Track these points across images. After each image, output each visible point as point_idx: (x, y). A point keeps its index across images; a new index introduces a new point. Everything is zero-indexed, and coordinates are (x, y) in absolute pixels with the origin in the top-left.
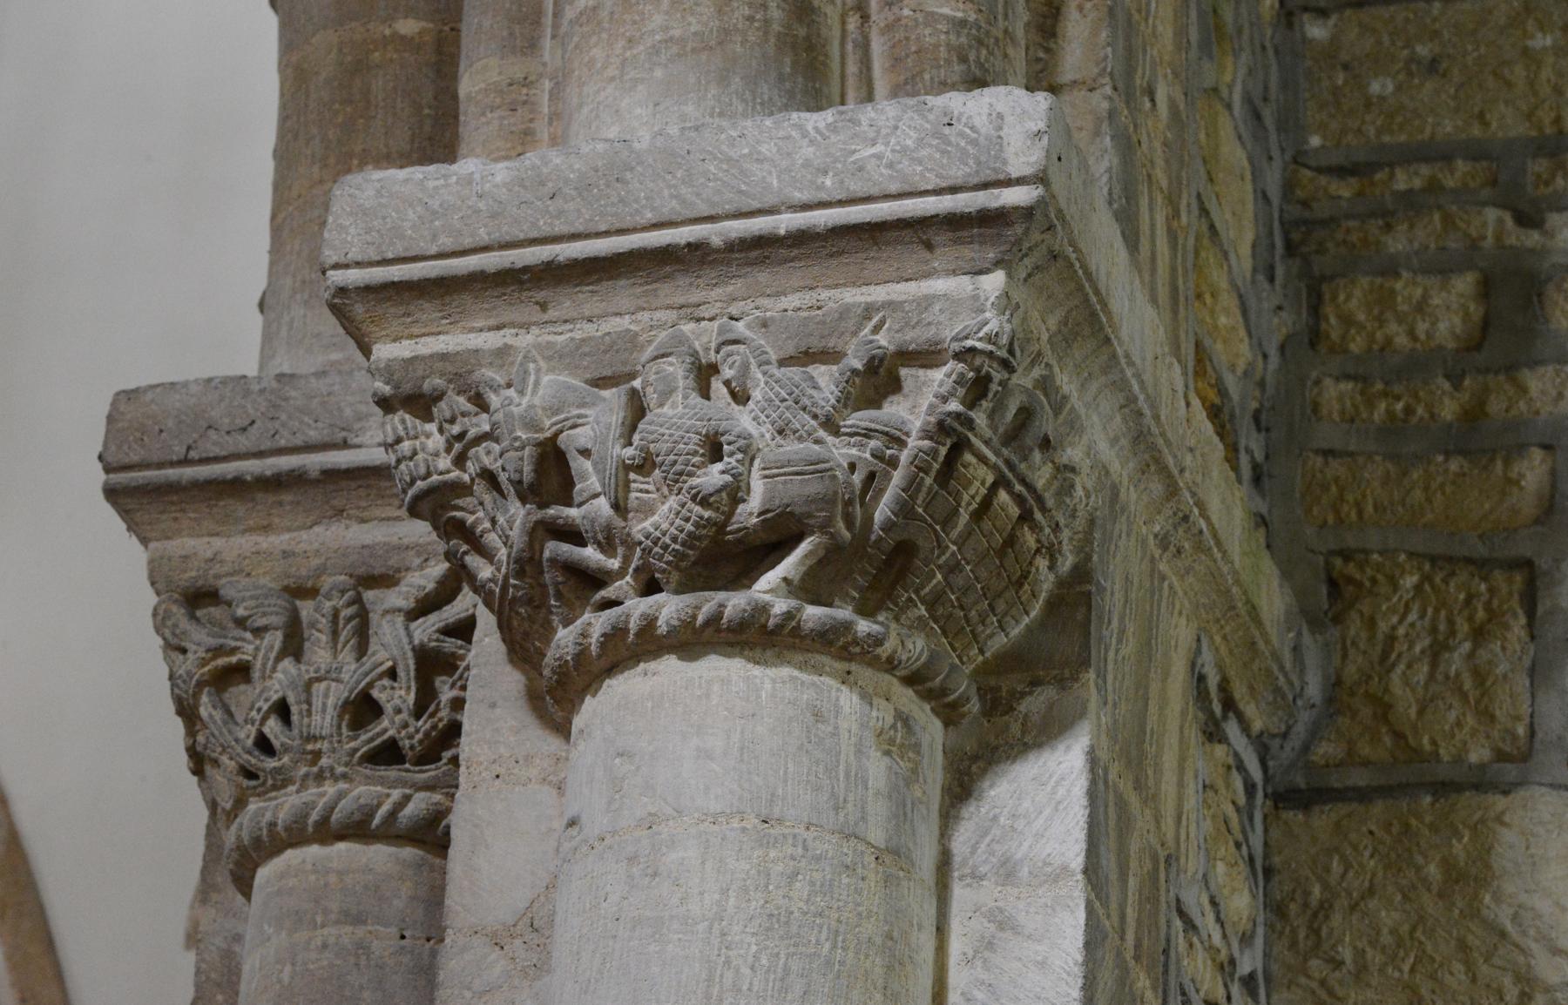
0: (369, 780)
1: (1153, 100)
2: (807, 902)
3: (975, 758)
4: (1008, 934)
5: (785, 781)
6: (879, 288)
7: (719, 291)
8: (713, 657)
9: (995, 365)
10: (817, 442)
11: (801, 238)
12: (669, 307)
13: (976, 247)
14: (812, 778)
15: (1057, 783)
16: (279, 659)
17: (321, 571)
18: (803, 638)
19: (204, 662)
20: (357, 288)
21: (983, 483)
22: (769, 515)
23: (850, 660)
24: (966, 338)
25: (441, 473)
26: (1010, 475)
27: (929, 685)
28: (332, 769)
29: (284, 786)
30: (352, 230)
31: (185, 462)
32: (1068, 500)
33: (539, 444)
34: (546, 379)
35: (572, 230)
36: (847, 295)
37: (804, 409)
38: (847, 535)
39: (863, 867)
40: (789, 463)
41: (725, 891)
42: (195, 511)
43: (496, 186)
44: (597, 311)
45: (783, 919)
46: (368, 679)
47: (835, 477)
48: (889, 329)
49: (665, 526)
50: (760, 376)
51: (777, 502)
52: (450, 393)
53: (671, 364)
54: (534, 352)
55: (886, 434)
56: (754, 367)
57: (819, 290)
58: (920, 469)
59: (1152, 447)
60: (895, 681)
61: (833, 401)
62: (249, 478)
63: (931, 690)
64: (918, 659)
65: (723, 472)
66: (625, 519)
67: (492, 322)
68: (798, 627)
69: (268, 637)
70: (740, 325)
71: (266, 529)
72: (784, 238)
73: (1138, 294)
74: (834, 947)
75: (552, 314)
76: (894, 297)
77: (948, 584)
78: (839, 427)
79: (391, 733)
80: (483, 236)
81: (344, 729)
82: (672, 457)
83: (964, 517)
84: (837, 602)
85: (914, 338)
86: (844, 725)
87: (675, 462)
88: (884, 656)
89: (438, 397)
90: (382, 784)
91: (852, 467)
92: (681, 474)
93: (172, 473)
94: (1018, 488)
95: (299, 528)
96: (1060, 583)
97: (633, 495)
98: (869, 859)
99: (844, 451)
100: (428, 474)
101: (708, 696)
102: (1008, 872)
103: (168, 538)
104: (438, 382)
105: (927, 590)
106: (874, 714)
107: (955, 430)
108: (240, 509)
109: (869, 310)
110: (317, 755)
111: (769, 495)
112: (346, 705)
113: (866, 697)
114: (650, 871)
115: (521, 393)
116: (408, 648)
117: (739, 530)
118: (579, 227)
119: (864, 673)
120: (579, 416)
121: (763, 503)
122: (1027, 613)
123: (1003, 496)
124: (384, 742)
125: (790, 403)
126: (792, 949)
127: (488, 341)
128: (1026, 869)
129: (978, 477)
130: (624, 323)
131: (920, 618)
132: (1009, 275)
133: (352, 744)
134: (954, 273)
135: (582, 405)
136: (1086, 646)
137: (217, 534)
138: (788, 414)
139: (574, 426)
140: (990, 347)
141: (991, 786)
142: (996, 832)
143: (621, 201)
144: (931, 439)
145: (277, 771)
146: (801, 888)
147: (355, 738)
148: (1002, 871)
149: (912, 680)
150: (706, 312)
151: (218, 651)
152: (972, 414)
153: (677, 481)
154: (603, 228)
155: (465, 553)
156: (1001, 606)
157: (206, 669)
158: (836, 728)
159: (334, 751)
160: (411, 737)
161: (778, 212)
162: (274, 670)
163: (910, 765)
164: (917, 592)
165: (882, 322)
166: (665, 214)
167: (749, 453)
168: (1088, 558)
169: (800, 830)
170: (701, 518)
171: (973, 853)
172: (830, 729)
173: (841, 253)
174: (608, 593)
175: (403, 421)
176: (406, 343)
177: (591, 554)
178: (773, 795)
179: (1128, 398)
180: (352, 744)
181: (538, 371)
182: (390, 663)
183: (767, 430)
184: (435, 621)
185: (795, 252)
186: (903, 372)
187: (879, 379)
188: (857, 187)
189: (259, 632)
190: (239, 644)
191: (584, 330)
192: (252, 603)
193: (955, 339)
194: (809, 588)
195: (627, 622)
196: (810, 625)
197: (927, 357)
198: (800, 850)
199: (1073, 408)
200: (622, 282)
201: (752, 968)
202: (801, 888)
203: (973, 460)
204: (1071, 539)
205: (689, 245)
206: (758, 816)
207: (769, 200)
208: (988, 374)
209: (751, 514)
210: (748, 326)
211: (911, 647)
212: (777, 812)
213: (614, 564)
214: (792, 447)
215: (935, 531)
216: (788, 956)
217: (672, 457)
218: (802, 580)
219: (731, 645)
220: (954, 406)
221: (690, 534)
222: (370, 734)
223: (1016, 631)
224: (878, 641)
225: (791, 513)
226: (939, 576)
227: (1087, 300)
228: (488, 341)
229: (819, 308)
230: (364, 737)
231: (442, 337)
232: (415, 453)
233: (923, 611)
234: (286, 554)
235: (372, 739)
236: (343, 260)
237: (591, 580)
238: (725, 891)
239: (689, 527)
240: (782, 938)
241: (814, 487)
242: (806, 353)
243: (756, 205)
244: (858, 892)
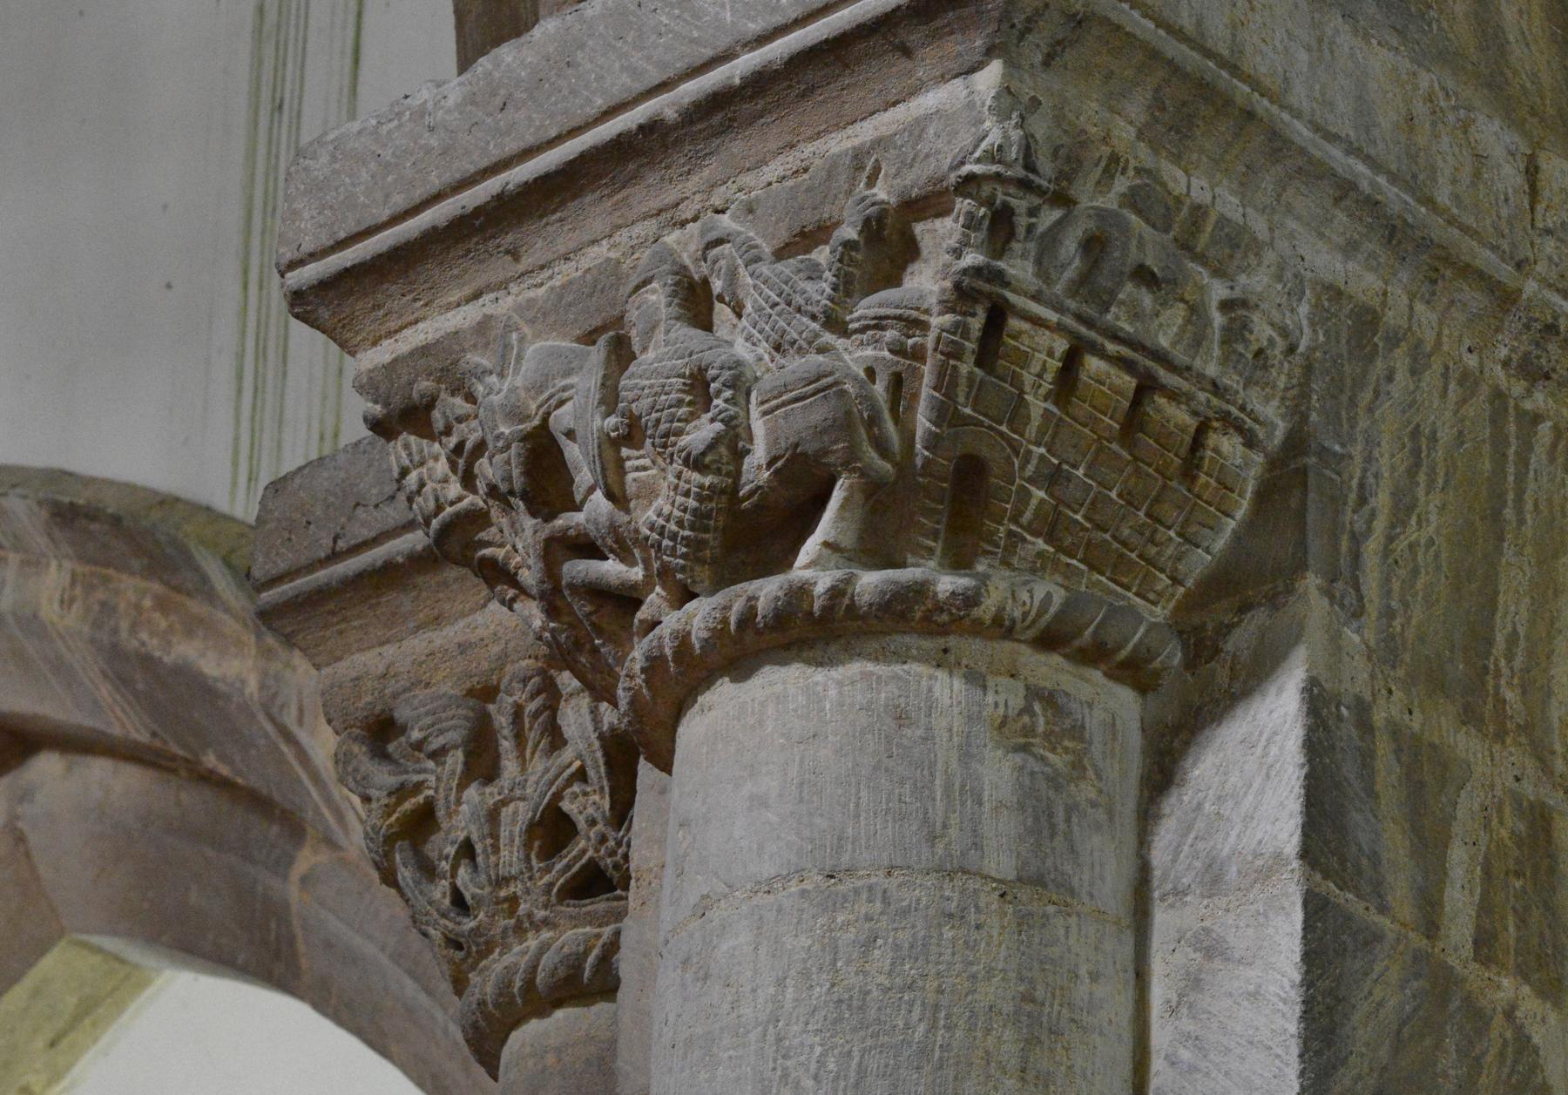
0: (576, 921)
2: (890, 974)
3: (1176, 729)
4: (1217, 963)
5: (857, 816)
6: (865, 124)
7: (695, 179)
8: (767, 669)
9: (1012, 190)
10: (821, 350)
11: (760, 83)
12: (646, 217)
13: (959, 37)
14: (894, 805)
15: (1269, 741)
16: (462, 786)
17: (503, 659)
18: (863, 618)
19: (389, 811)
20: (312, 287)
21: (1050, 354)
22: (779, 464)
24: (962, 163)
25: (452, 504)
26: (1093, 335)
27: (1077, 643)
28: (530, 915)
29: (491, 952)
30: (306, 215)
31: (334, 556)
32: (1240, 348)
33: (525, 438)
35: (522, 145)
36: (833, 143)
37: (799, 310)
39: (978, 910)
40: (786, 388)
41: (781, 983)
42: (359, 617)
43: (449, 111)
44: (572, 245)
45: (855, 1003)
46: (554, 789)
47: (843, 393)
48: (886, 175)
49: (667, 509)
50: (749, 280)
51: (783, 445)
52: (443, 395)
53: (654, 291)
54: (516, 318)
55: (899, 318)
56: (741, 270)
57: (801, 146)
58: (948, 355)
59: (1425, 244)
60: (1023, 648)
61: (828, 290)
62: (400, 559)
63: (1081, 650)
64: (1040, 614)
65: (712, 420)
66: (627, 511)
67: (468, 291)
68: (852, 607)
69: (449, 760)
70: (725, 219)
71: (437, 621)
72: (742, 87)
74: (933, 1027)
75: (526, 262)
76: (885, 131)
77: (1060, 501)
78: (847, 323)
79: (590, 853)
80: (435, 182)
81: (534, 861)
82: (654, 415)
83: (1037, 406)
84: (910, 559)
85: (915, 180)
86: (940, 724)
87: (658, 421)
88: (988, 618)
89: (431, 404)
90: (590, 923)
91: (871, 373)
92: (666, 435)
93: (322, 575)
94: (1111, 347)
95: (473, 611)
96: (1273, 463)
97: (630, 476)
98: (990, 900)
99: (859, 354)
100: (439, 508)
101: (761, 723)
102: (1213, 879)
103: (339, 659)
104: (425, 385)
106: (990, 699)
107: (980, 292)
108: (405, 601)
109: (858, 158)
110: (513, 900)
111: (773, 442)
112: (532, 829)
113: (976, 679)
114: (702, 973)
115: (502, 375)
116: (594, 736)
117: (751, 493)
118: (530, 139)
119: (971, 648)
120: (564, 389)
124: (583, 867)
125: (783, 306)
126: (869, 1042)
127: (464, 317)
128: (1234, 869)
129: (1043, 350)
130: (601, 252)
132: (1011, 64)
133: (547, 878)
134: (944, 78)
135: (568, 373)
137: (388, 641)
138: (782, 323)
139: (561, 403)
140: (994, 168)
141: (1195, 764)
142: (1200, 825)
143: (573, 92)
144: (952, 310)
145: (475, 932)
146: (881, 956)
147: (548, 870)
148: (1207, 878)
149: (1048, 641)
150: (687, 211)
151: (401, 793)
152: (1001, 264)
153: (665, 446)
154: (553, 133)
156: (1169, 512)
157: (393, 818)
158: (929, 729)
159: (528, 892)
160: (612, 853)
161: (736, 56)
162: (459, 802)
163: (1069, 758)
164: (1015, 519)
165: (877, 170)
166: (618, 95)
167: (740, 384)
168: (1305, 418)
169: (879, 879)
170: (701, 487)
171: (1174, 861)
172: (920, 732)
173: (812, 89)
174: (643, 613)
175: (407, 447)
176: (386, 343)
177: (611, 569)
178: (840, 839)
180: (547, 878)
181: (522, 340)
182: (577, 764)
183: (764, 349)
185: (761, 104)
186: (919, 228)
187: (887, 245)
189: (438, 755)
190: (421, 777)
191: (566, 272)
192: (428, 720)
193: (954, 168)
194: (875, 548)
195: (661, 647)
196: (866, 598)
197: (928, 204)
198: (878, 905)
200: (588, 199)
201: (816, 1078)
202: (881, 956)
203: (1026, 326)
205: (641, 127)
207: (723, 43)
208: (1005, 205)
209: (759, 467)
210: (734, 218)
211: (1025, 596)
212: (845, 859)
213: (637, 573)
214: (798, 365)
215: (1001, 434)
216: (863, 1051)
217: (654, 415)
218: (861, 539)
219: (787, 647)
220: (971, 259)
221: (695, 511)
222: (565, 861)
223: (1220, 544)
224: (970, 600)
225: (804, 454)
227: (1174, 68)
228: (464, 317)
229: (806, 170)
230: (558, 867)
231: (421, 326)
232: (422, 484)
233: (1041, 544)
234: (463, 648)
235: (568, 867)
236: (297, 256)
237: (625, 600)
238: (781, 983)
239: (692, 503)
240: (854, 1030)
241: (818, 413)
242: (802, 234)
243: (708, 53)
244: (970, 946)
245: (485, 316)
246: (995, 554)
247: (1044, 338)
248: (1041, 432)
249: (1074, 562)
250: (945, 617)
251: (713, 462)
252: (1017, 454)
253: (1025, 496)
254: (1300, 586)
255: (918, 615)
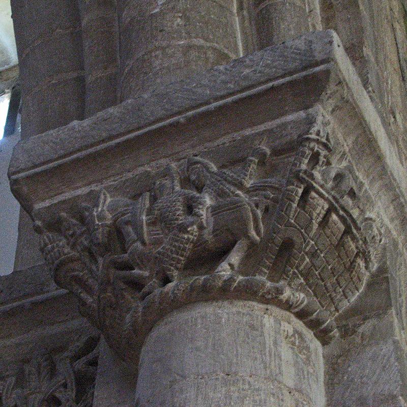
1: (394, 117)
21: (323, 208)
23: (267, 304)
34: (109, 200)
38: (258, 238)
60: (292, 316)
64: (302, 303)
72: (215, 111)
73: (396, 172)
77: (313, 265)
88: (284, 300)
94: (341, 213)
96: (373, 276)
105: (302, 267)
121: (214, 227)
122: (358, 290)
123: (334, 217)
131: (301, 284)
136: (389, 298)
155: (81, 293)
161: (210, 103)
164: (297, 268)
168: (385, 263)
179: (395, 195)
184: (84, 359)
188: (244, 84)
199: (366, 190)
203: (317, 196)
204: (375, 257)
206: (224, 372)
213: (147, 274)
223: (353, 300)
226: (308, 260)
233: (302, 280)
245: (91, 190)
246: (287, 280)
247: (321, 201)
248: (315, 235)
249: (310, 290)
250: (270, 296)
251: (222, 358)
252: (305, 241)
253: (303, 260)
254: (389, 312)
255: (261, 294)
